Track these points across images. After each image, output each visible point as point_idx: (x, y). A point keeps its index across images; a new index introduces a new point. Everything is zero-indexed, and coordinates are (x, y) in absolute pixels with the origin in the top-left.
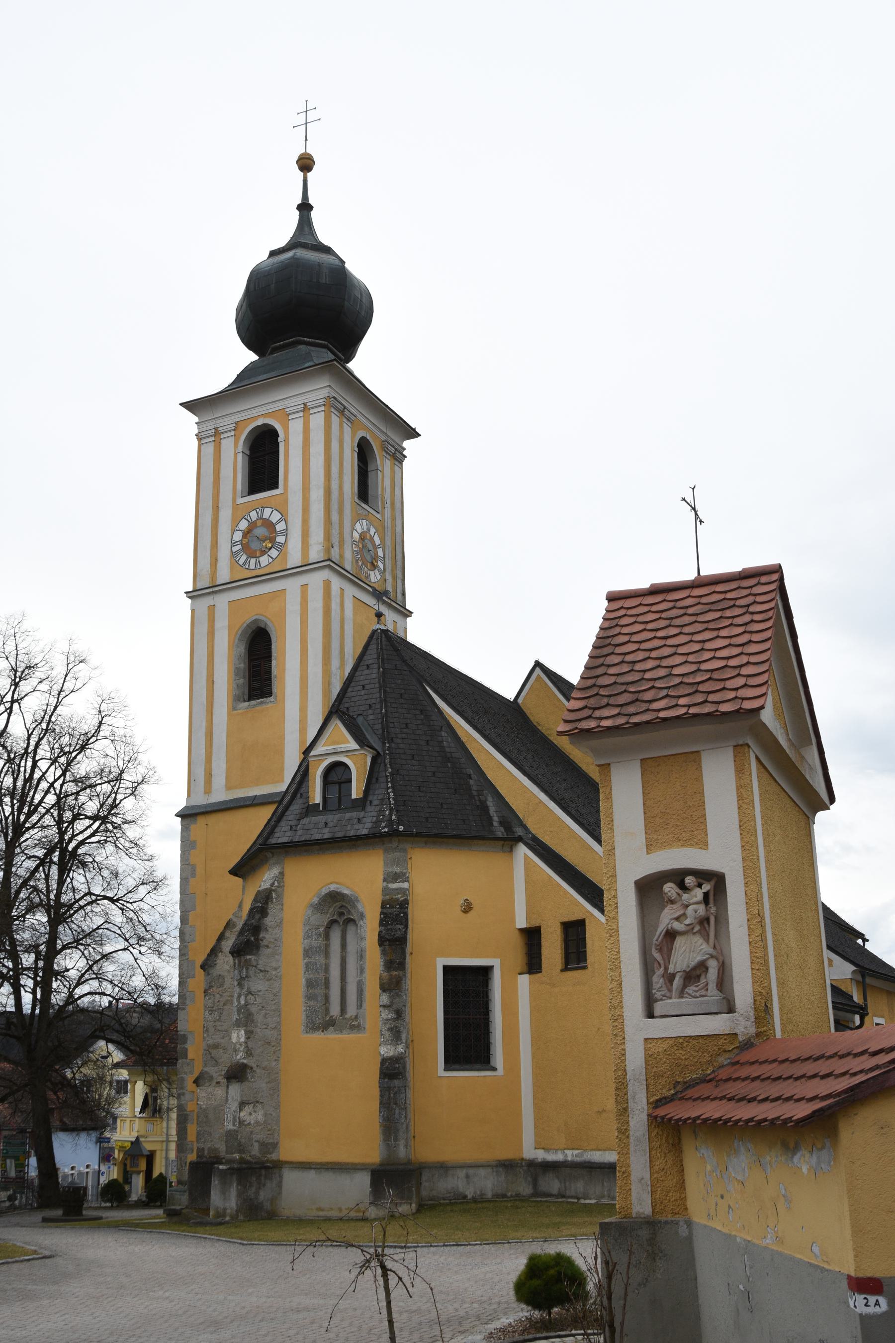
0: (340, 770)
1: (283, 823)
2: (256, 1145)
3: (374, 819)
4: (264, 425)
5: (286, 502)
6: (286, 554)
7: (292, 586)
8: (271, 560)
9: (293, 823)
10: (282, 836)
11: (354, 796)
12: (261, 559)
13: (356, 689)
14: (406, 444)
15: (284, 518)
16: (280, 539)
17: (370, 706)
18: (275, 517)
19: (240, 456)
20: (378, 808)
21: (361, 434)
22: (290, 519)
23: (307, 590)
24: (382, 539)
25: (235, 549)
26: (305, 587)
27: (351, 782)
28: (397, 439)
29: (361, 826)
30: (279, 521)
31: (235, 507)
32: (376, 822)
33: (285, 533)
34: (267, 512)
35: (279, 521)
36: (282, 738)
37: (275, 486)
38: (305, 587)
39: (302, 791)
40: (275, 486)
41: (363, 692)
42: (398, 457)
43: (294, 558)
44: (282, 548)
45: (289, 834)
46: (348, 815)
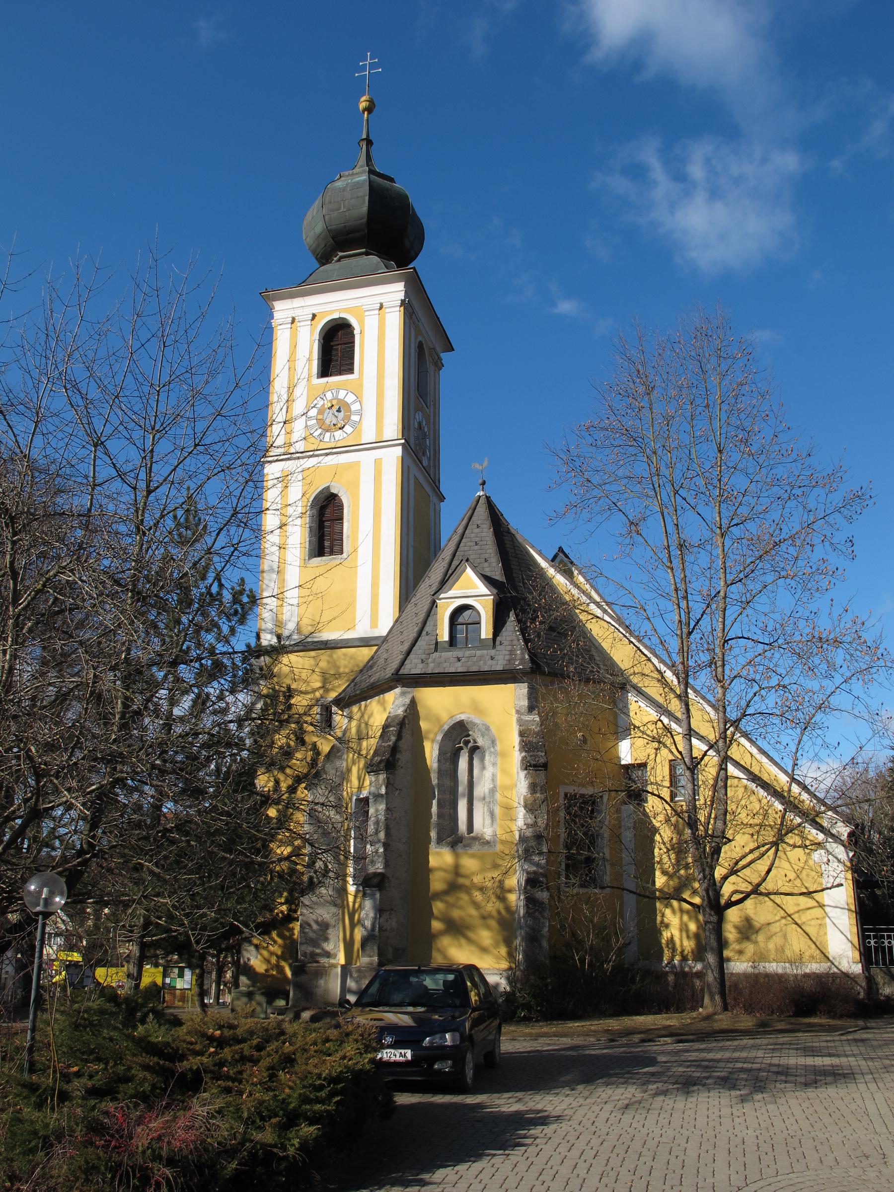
0: (467, 613)
1: (411, 656)
2: (390, 950)
3: (507, 657)
4: (340, 318)
5: (361, 386)
6: (360, 431)
7: (366, 459)
8: (345, 435)
9: (423, 657)
10: (414, 667)
11: (483, 636)
12: (336, 433)
13: (468, 544)
14: (445, 356)
15: (359, 399)
16: (355, 418)
17: (486, 560)
18: (350, 398)
19: (316, 343)
20: (509, 648)
21: (420, 338)
22: (364, 402)
23: (381, 463)
24: (429, 431)
25: (309, 423)
26: (378, 463)
27: (479, 623)
28: (438, 349)
29: (494, 662)
30: (354, 402)
31: (310, 387)
32: (509, 660)
33: (360, 413)
34: (342, 394)
35: (354, 402)
36: (354, 591)
37: (351, 371)
38: (378, 463)
39: (428, 628)
40: (351, 371)
41: (476, 548)
42: (439, 365)
43: (368, 435)
44: (356, 426)
45: (421, 666)
46: (479, 653)
